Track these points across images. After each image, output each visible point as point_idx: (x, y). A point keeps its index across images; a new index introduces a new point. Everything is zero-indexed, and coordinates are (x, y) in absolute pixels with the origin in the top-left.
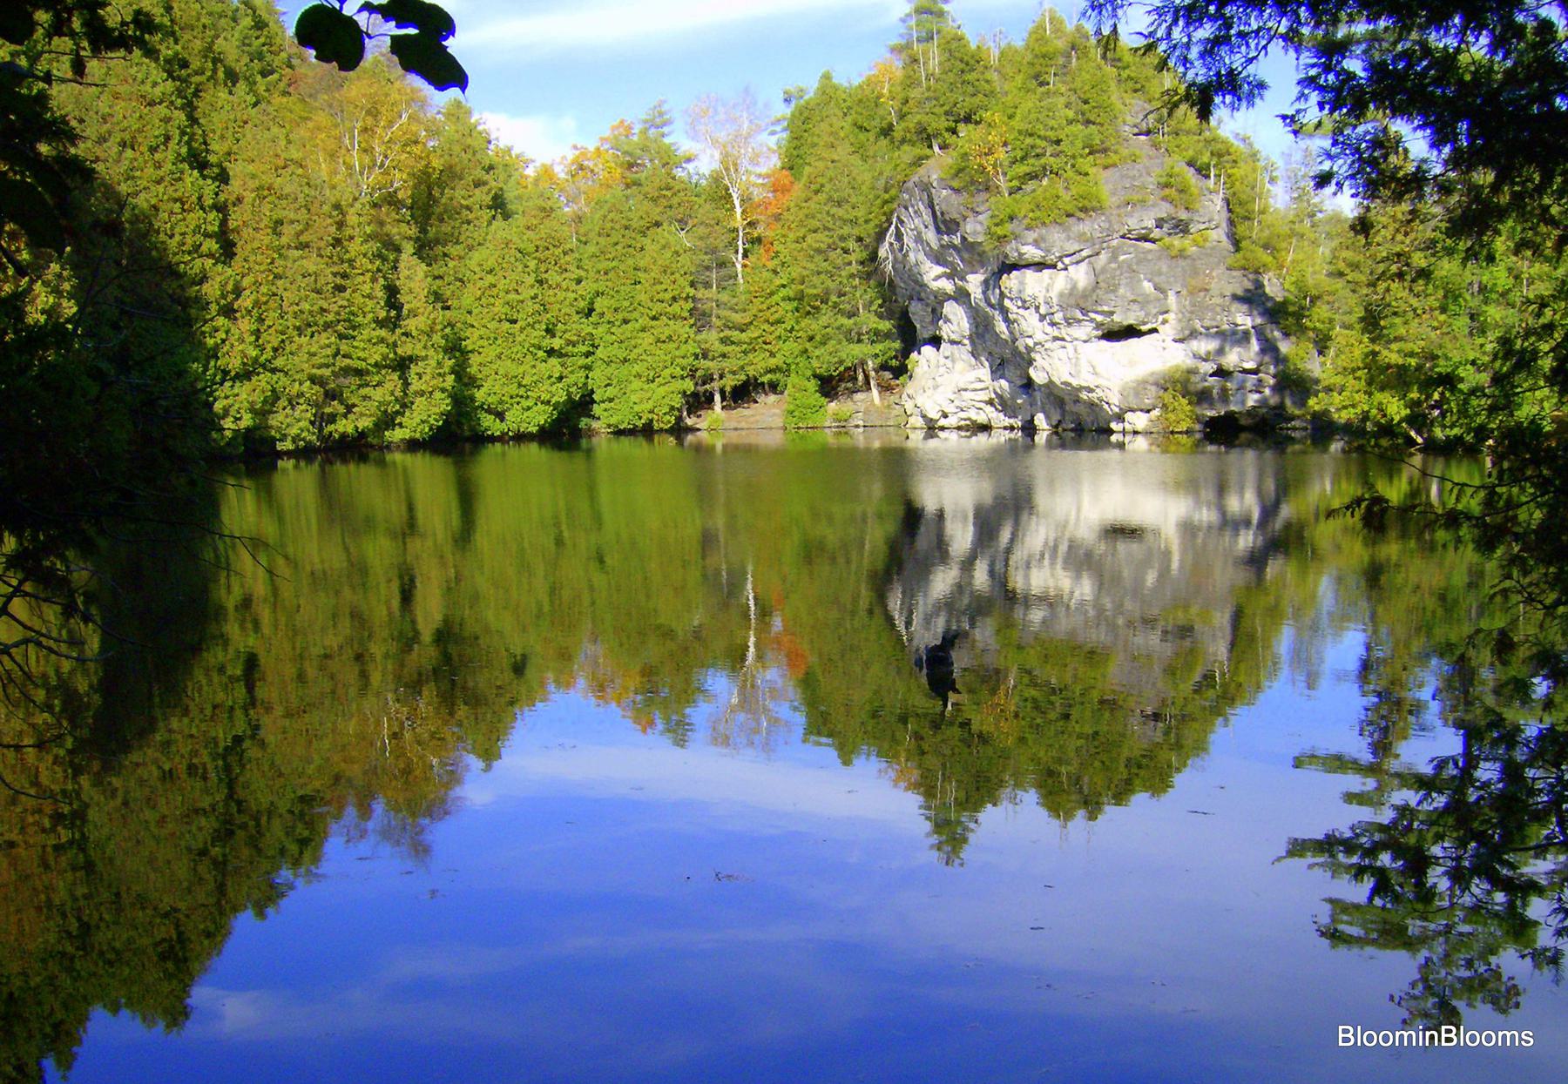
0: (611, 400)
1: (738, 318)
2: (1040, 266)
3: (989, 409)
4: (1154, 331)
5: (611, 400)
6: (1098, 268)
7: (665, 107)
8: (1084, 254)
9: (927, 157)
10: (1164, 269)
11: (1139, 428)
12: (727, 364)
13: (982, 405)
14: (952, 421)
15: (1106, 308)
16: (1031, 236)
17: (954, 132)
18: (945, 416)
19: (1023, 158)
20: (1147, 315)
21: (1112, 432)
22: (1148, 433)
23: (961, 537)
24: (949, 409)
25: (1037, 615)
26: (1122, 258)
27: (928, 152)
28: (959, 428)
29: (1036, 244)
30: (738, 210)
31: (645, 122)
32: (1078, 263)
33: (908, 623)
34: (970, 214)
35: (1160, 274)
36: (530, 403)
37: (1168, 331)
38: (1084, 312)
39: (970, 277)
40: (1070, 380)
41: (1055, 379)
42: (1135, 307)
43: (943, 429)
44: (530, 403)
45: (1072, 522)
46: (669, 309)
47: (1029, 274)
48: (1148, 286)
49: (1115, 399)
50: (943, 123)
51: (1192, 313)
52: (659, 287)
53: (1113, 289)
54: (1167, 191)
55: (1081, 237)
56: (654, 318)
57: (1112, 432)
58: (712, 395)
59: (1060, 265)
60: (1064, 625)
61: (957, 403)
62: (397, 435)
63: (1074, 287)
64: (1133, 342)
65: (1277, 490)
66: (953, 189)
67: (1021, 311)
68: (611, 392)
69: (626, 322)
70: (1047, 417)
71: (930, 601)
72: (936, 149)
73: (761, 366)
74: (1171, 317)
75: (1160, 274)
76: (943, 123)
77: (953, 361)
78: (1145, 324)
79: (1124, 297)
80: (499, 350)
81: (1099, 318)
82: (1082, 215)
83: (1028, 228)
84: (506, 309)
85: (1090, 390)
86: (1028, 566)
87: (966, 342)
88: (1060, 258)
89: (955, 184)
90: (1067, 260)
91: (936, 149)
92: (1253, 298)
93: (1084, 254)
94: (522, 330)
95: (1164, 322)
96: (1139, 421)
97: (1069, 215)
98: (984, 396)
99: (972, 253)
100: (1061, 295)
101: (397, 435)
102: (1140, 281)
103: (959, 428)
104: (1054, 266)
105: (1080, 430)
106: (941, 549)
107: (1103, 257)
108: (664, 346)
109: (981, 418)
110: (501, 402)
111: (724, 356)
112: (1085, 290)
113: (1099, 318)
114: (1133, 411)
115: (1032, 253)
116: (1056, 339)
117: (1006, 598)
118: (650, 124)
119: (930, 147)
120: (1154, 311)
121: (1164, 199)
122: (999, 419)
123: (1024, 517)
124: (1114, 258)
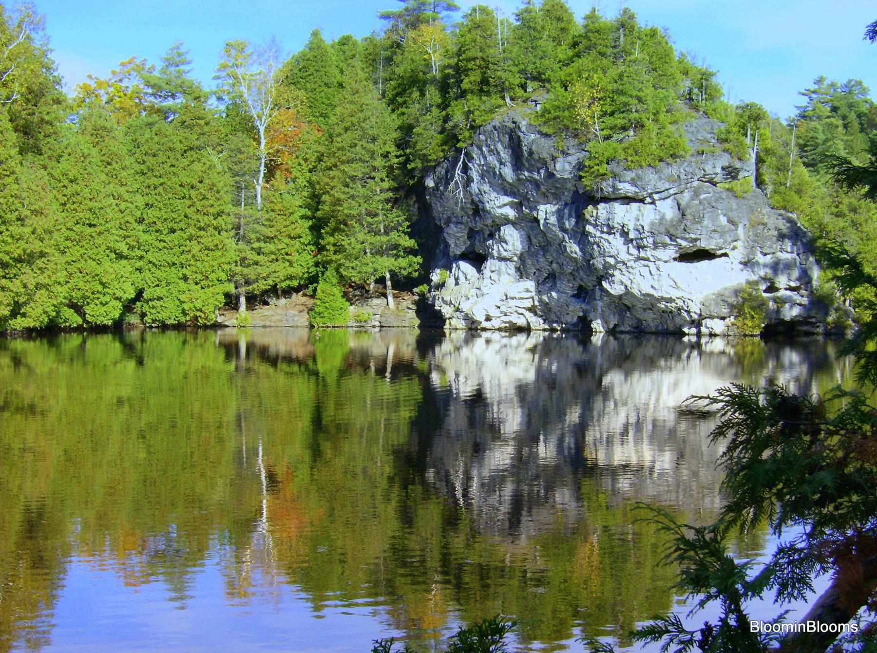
0: (159, 299)
1: (269, 232)
2: (627, 200)
3: (528, 314)
4: (725, 255)
5: (159, 299)
6: (683, 203)
7: (183, 49)
8: (672, 192)
9: (500, 106)
10: (734, 206)
11: (718, 331)
12: (263, 271)
13: (523, 311)
14: (496, 323)
15: (693, 236)
16: (630, 175)
17: (524, 87)
18: (488, 319)
19: (612, 114)
20: (725, 242)
21: (684, 334)
22: (725, 336)
23: (512, 420)
24: (494, 312)
25: (624, 484)
26: (702, 196)
27: (501, 102)
28: (500, 330)
29: (633, 182)
30: (263, 142)
31: (166, 60)
32: (664, 199)
33: (465, 495)
34: (560, 155)
35: (732, 210)
36: (107, 298)
37: (737, 255)
38: (672, 237)
39: (542, 208)
40: (652, 292)
41: (635, 291)
42: (716, 235)
43: (484, 329)
44: (107, 298)
45: (651, 406)
46: (215, 222)
47: (617, 207)
48: (723, 220)
49: (695, 308)
50: (517, 80)
51: (755, 241)
52: (205, 202)
53: (698, 220)
54: (727, 145)
55: (669, 179)
56: (201, 229)
57: (684, 334)
58: (237, 298)
59: (648, 200)
60: (650, 490)
61: (503, 309)
62: (19, 323)
63: (663, 218)
64: (705, 263)
65: (810, 386)
66: (540, 133)
67: (605, 236)
68: (158, 292)
69: (173, 231)
70: (605, 322)
71: (486, 473)
72: (508, 100)
73: (282, 274)
74: (739, 244)
75: (732, 210)
76: (517, 80)
77: (499, 274)
78: (721, 249)
79: (707, 227)
80: (83, 251)
81: (684, 244)
82: (670, 160)
83: (628, 169)
84: (88, 215)
85: (670, 300)
86: (609, 442)
87: (516, 259)
88: (650, 195)
89: (545, 130)
90: (656, 197)
91: (508, 100)
92: (795, 234)
93: (672, 192)
94: (100, 234)
95: (734, 248)
96: (718, 326)
97: (661, 160)
98: (528, 304)
99: (552, 188)
100: (652, 224)
101: (19, 323)
102: (718, 215)
103: (500, 330)
104: (642, 201)
105: (639, 332)
106: (495, 430)
107: (687, 195)
108: (211, 253)
109: (521, 322)
110: (84, 297)
111: (256, 263)
112: (672, 221)
113: (684, 244)
114: (711, 317)
115: (626, 188)
116: (639, 259)
117: (578, 466)
118: (170, 63)
119: (503, 98)
120: (730, 239)
121: (725, 151)
122: (537, 322)
123: (598, 404)
124: (696, 193)
